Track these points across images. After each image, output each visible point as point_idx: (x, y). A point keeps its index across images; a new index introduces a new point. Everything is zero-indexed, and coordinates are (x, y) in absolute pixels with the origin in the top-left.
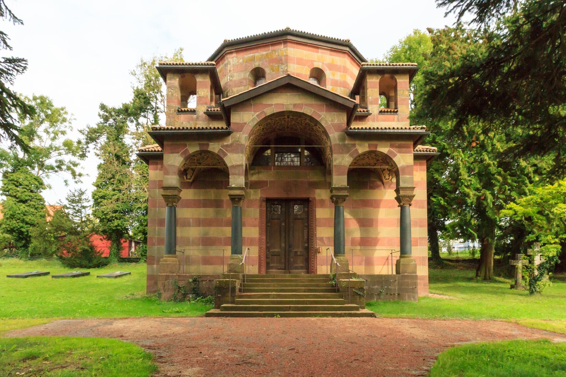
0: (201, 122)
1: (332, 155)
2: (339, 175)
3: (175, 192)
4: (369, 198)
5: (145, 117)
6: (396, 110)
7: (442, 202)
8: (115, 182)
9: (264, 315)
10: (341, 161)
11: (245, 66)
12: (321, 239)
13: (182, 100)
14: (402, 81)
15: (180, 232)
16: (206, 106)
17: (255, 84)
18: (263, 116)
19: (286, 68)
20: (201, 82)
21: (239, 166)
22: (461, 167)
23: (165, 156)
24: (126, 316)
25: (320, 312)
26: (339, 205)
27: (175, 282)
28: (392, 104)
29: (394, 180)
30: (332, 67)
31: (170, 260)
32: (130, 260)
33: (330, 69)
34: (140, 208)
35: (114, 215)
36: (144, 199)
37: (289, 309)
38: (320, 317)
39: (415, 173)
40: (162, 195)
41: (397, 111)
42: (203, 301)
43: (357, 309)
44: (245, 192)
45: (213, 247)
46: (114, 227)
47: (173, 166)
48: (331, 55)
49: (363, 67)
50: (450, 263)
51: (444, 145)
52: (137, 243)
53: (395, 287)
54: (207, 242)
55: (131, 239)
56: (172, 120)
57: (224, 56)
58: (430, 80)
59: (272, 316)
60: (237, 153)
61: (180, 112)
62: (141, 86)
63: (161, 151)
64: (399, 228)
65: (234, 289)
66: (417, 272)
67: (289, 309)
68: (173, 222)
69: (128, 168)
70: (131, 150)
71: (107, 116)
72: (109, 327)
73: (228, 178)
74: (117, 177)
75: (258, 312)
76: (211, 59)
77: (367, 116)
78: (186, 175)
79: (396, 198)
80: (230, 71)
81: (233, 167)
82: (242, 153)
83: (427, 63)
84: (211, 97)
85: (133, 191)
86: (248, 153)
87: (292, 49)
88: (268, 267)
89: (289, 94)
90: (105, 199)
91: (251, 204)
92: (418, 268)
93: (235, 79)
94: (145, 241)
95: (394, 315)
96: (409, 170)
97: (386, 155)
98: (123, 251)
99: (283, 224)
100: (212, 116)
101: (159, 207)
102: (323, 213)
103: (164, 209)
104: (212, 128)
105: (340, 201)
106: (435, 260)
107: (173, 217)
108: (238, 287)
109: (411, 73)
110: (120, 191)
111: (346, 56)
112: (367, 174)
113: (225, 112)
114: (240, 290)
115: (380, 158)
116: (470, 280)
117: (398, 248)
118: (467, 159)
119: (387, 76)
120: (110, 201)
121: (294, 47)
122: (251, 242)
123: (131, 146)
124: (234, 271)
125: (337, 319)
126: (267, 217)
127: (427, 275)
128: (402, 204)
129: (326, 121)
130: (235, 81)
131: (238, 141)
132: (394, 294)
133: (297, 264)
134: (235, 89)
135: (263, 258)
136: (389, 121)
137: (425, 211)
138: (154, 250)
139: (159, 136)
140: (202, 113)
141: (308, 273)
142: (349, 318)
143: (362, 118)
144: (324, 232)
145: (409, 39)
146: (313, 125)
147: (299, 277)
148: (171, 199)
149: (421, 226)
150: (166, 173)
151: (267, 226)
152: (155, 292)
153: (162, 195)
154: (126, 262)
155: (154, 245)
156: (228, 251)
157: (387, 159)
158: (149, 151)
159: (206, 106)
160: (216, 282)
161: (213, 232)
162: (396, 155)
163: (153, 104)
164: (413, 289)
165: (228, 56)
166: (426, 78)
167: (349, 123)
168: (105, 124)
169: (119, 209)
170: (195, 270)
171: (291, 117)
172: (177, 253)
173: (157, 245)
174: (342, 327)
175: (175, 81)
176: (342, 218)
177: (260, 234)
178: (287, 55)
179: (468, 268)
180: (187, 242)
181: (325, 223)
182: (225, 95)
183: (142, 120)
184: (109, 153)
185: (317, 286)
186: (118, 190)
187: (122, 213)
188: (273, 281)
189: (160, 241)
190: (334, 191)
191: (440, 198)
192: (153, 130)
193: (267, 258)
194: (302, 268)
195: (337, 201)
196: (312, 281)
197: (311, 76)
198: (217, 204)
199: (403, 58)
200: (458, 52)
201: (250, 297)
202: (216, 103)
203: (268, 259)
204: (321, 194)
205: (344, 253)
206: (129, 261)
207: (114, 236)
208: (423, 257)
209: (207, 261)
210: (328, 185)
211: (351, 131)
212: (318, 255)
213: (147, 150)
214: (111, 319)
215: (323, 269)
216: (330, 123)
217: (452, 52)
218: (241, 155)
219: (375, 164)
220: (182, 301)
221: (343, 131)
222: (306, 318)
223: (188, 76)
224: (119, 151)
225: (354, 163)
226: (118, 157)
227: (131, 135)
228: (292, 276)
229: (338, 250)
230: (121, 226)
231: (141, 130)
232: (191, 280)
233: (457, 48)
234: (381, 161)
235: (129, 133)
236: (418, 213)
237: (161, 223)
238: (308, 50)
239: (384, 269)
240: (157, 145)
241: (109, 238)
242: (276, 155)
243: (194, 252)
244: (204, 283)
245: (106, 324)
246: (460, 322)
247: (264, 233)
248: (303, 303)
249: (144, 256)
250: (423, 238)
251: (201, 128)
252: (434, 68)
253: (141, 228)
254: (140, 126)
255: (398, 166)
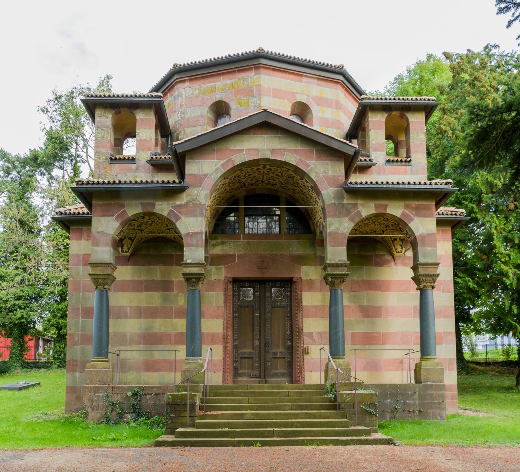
0: (142, 175)
1: (325, 219)
2: (334, 246)
3: (108, 271)
4: (378, 279)
5: (61, 168)
6: (408, 159)
7: (471, 284)
8: (19, 258)
9: (238, 444)
10: (338, 227)
11: (203, 99)
12: (310, 335)
13: (116, 145)
14: (416, 120)
15: (115, 326)
16: (149, 152)
17: (216, 123)
18: (231, 166)
19: (258, 102)
20: (142, 120)
21: (197, 233)
22: (495, 237)
23: (94, 220)
24: (41, 447)
25: (317, 438)
26: (336, 287)
27: (108, 397)
28: (403, 152)
29: (410, 253)
30: (321, 101)
31: (101, 365)
32: (36, 365)
33: (318, 105)
34: (52, 293)
35: (17, 302)
36: (59, 280)
37: (273, 434)
38: (317, 445)
39: (439, 245)
40: (89, 274)
41: (410, 161)
42: (145, 423)
43: (368, 433)
44: (205, 269)
45: (160, 347)
46: (17, 319)
47: (106, 234)
48: (318, 85)
49: (364, 101)
50: (478, 367)
51: (473, 208)
52: (47, 341)
53: (414, 402)
54: (151, 339)
55: (38, 335)
56: (103, 171)
57: (173, 86)
58: (477, 115)
59: (249, 444)
60: (195, 215)
61: (113, 160)
62: (57, 126)
63: (88, 214)
64: (418, 320)
65: (193, 405)
66: (445, 380)
67: (273, 434)
68: (105, 312)
69: (37, 238)
70: (41, 213)
71: (8, 167)
72: (20, 462)
73: (182, 250)
74: (22, 250)
75: (229, 439)
76: (157, 89)
77: (370, 167)
78: (122, 248)
79: (413, 278)
80: (181, 105)
81: (188, 234)
82: (201, 215)
83: (443, 98)
84: (156, 140)
85: (43, 269)
86: (209, 216)
87: (266, 77)
88: (236, 373)
89: (265, 136)
90: (4, 281)
91: (212, 287)
92: (446, 373)
93: (188, 116)
94: (61, 338)
95: (419, 442)
96: (430, 239)
97: (399, 218)
98: (28, 353)
99: (257, 314)
100: (158, 166)
101: (84, 291)
102: (312, 299)
103: (91, 293)
104: (160, 181)
105: (337, 281)
106: (463, 365)
107: (105, 304)
108: (198, 403)
109: (428, 110)
110: (25, 269)
111: (339, 86)
112: (370, 246)
113: (177, 160)
114: (201, 408)
115: (390, 223)
116: (509, 389)
117: (418, 347)
118: (503, 226)
119: (394, 113)
120: (11, 284)
121: (269, 75)
122: (213, 339)
123: (41, 208)
124: (191, 380)
125: (342, 448)
126: (234, 305)
127: (457, 384)
128: (422, 286)
129: (317, 173)
130: (189, 119)
131: (195, 200)
132: (414, 411)
133: (277, 369)
134: (188, 130)
135: (230, 363)
136: (399, 173)
137: (452, 295)
138: (74, 351)
139: (87, 194)
140: (144, 161)
141: (292, 382)
142: (357, 447)
143: (364, 169)
144: (314, 326)
145: (419, 65)
146: (299, 178)
147: (283, 388)
148: (102, 281)
149: (445, 317)
150: (96, 244)
151: (234, 317)
152: (77, 410)
153: (89, 274)
154: (32, 368)
155: (76, 344)
156: (181, 352)
157: (399, 225)
158: (70, 214)
159: (149, 152)
160: (167, 397)
161: (159, 325)
162: (413, 219)
163: (73, 151)
164: (439, 403)
165: (179, 86)
166: (471, 113)
167: (347, 175)
168: (6, 179)
169: (24, 294)
170: (134, 379)
171: (268, 167)
172: (110, 354)
173: (81, 344)
174: (352, 459)
175: (106, 118)
176: (340, 306)
177: (225, 328)
178: (260, 85)
179: (501, 373)
180: (123, 340)
181: (317, 312)
182: (175, 139)
183: (56, 172)
184: (11, 218)
185: (309, 401)
186: (23, 269)
187: (27, 299)
188: (246, 394)
189: (86, 339)
190: (328, 268)
191: (467, 279)
192: (77, 184)
193: (234, 362)
194: (283, 375)
195: (333, 281)
196: (301, 393)
197: (292, 114)
198: (165, 286)
199: (411, 91)
200: (486, 85)
201: (215, 417)
202: (162, 149)
203: (236, 363)
204: (310, 273)
205: (344, 355)
206: (36, 367)
207: (16, 331)
208: (450, 359)
209: (150, 366)
210: (321, 260)
211: (351, 186)
212: (306, 357)
213: (68, 212)
214: (20, 451)
215: (313, 377)
216: (321, 175)
217: (478, 84)
218: (200, 219)
219: (383, 231)
220: (116, 423)
221: (340, 186)
222: (297, 447)
223: (124, 112)
224: (24, 214)
225: (354, 230)
226: (23, 224)
227: (41, 193)
228: (273, 388)
229: (336, 350)
230: (26, 318)
231: (55, 185)
232: (130, 394)
233: (484, 79)
234: (391, 227)
235: (39, 190)
236: (443, 298)
237: (87, 313)
238: (289, 79)
239: (402, 377)
240: (82, 205)
241: (9, 335)
242: (247, 219)
243: (133, 354)
244: (148, 397)
245: (14, 457)
246: (511, 450)
247: (230, 326)
248: (292, 425)
249: (61, 361)
250: (449, 333)
251: (144, 181)
252: (454, 105)
253: (54, 321)
254: (53, 181)
255: (417, 234)
